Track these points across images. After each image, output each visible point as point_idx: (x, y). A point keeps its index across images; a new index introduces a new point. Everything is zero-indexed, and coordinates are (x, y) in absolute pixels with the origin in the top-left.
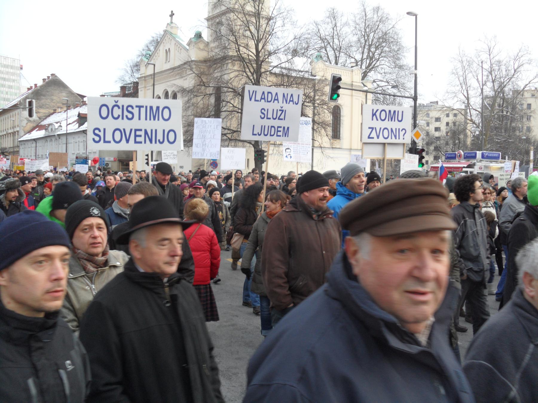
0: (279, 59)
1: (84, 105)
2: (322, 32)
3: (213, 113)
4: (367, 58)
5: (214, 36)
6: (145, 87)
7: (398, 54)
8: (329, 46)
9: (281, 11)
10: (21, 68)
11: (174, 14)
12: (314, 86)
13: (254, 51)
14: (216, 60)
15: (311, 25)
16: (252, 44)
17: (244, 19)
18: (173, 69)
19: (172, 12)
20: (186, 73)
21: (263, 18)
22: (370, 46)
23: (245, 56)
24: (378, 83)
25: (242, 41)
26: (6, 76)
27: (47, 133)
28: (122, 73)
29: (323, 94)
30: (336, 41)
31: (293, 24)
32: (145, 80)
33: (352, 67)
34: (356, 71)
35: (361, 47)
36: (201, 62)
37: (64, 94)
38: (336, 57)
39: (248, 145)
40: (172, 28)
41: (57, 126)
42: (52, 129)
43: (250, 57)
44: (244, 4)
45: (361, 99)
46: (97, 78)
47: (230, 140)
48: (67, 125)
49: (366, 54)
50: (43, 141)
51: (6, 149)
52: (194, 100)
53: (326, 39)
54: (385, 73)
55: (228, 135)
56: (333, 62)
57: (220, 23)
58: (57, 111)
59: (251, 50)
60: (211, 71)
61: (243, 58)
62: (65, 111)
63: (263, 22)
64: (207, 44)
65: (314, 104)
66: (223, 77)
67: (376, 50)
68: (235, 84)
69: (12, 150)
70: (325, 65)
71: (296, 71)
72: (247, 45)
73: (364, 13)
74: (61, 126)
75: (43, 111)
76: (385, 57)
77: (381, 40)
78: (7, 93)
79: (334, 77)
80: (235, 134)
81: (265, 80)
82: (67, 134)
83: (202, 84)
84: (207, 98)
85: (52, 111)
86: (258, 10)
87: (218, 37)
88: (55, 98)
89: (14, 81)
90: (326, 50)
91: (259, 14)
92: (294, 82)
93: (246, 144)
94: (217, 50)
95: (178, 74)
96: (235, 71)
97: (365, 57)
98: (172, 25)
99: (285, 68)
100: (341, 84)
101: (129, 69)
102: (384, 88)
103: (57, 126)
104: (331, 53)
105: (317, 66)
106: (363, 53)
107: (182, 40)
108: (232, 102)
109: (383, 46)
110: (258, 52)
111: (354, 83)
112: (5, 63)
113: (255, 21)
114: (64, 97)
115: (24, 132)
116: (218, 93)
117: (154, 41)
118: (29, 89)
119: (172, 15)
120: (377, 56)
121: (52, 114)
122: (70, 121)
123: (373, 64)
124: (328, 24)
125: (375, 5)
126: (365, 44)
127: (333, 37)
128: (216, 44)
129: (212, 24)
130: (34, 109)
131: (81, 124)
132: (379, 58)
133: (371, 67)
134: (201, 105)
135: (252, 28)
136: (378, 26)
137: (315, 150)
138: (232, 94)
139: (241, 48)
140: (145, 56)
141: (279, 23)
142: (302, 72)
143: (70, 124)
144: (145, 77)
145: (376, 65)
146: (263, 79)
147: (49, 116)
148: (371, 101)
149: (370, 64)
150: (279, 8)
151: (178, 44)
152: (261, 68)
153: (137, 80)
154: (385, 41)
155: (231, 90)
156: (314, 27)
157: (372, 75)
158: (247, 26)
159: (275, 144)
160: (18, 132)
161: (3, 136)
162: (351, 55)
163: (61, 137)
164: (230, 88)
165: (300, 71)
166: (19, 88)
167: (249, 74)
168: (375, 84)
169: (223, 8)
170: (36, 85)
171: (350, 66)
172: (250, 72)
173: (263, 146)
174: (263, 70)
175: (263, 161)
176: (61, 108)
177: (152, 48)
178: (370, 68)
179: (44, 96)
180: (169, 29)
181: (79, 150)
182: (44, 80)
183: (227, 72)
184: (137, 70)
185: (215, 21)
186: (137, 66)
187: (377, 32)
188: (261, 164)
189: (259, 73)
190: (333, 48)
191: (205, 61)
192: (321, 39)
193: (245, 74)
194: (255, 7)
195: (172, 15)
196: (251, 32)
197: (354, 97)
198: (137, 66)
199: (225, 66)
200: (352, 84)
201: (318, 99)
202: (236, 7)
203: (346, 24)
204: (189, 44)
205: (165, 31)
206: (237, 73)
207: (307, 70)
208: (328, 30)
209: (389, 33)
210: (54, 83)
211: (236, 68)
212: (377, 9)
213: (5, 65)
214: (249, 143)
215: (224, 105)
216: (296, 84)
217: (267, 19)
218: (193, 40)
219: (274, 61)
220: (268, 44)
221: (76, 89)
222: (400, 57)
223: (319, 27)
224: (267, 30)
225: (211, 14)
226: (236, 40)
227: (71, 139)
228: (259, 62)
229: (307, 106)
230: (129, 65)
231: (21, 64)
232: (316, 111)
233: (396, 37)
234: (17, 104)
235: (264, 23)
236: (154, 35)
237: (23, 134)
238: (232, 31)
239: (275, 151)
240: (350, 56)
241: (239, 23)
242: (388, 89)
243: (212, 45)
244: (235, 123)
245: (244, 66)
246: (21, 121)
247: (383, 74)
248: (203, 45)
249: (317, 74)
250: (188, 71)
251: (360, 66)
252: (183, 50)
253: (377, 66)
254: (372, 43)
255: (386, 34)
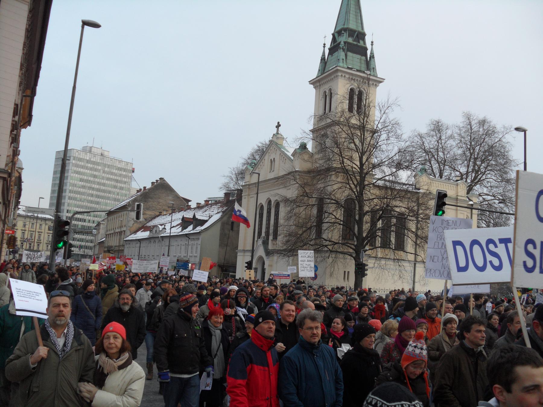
0: (383, 172)
1: (188, 209)
2: (426, 144)
3: (315, 224)
4: (473, 172)
5: (319, 148)
6: (249, 195)
7: (505, 167)
8: (433, 159)
9: (386, 125)
10: (133, 171)
11: (280, 126)
12: (418, 199)
13: (358, 163)
14: (320, 171)
15: (416, 138)
16: (356, 156)
17: (349, 132)
18: (277, 178)
19: (278, 123)
20: (290, 183)
21: (368, 130)
22: (476, 159)
23: (349, 168)
24: (484, 197)
25: (346, 153)
26: (119, 179)
27: (151, 234)
28: (226, 180)
29: (427, 208)
30: (441, 154)
31: (398, 137)
32: (249, 188)
33: (457, 181)
34: (461, 185)
35: (466, 160)
36: (304, 172)
37: (170, 198)
38: (441, 170)
39: (349, 257)
40: (278, 138)
41: (161, 228)
42: (156, 231)
43: (354, 169)
44: (349, 118)
45: (466, 213)
46: (202, 182)
47: (331, 251)
48: (171, 228)
49: (472, 168)
50: (147, 242)
51: (112, 247)
52: (296, 210)
53: (430, 152)
54: (491, 187)
55: (329, 247)
56: (438, 175)
57: (325, 136)
58: (162, 214)
59: (355, 162)
60: (315, 182)
61: (347, 170)
62: (170, 214)
63: (368, 135)
64: (312, 155)
65: (417, 218)
66: (326, 188)
67: (482, 164)
68: (338, 196)
69: (117, 249)
70: (429, 178)
71: (400, 184)
72: (351, 157)
73: (469, 127)
74: (165, 228)
75: (150, 213)
76: (491, 170)
77: (487, 154)
78: (118, 194)
79: (439, 193)
80: (336, 246)
81: (368, 193)
82: (170, 237)
83: (306, 194)
84: (310, 209)
85: (158, 214)
86: (363, 123)
87: (321, 148)
88: (161, 201)
89: (125, 183)
90: (430, 163)
91: (364, 127)
92: (397, 196)
93: (347, 256)
94: (321, 162)
95: (282, 184)
96: (339, 182)
97: (470, 170)
98: (279, 136)
99: (389, 181)
100: (447, 201)
101: (234, 176)
102: (490, 202)
103: (161, 228)
104: (435, 166)
105: (421, 180)
106: (468, 166)
107: (288, 152)
108: (334, 213)
109: (489, 160)
110: (362, 164)
111: (459, 198)
112: (119, 166)
113: (359, 134)
114: (170, 200)
115: (130, 232)
116: (321, 204)
117: (259, 150)
118: (138, 191)
119: (278, 126)
120: (483, 170)
121: (158, 216)
122: (174, 224)
123: (479, 177)
124: (433, 137)
125: (481, 117)
126: (471, 157)
127: (437, 149)
128: (321, 155)
129: (317, 137)
130: (142, 212)
131: (184, 228)
132: (485, 172)
133: (477, 180)
134: (303, 215)
135: (357, 141)
136: (484, 139)
137: (417, 265)
138: (334, 206)
139: (345, 160)
140: (250, 165)
141: (384, 136)
142: (406, 185)
143: (174, 227)
144: (249, 185)
145: (482, 179)
146: (366, 192)
147: (155, 218)
148: (476, 216)
149: (475, 178)
150: (384, 122)
151: (284, 155)
152: (364, 180)
153: (241, 187)
154: (491, 154)
155: (334, 202)
156: (419, 140)
157: (478, 188)
158: (351, 139)
159: (376, 258)
160: (124, 231)
161: (111, 234)
162: (456, 168)
163: (165, 240)
164: (332, 199)
165: (404, 184)
166: (129, 190)
167: (352, 186)
168: (481, 199)
169: (329, 121)
170: (145, 188)
171: (455, 179)
172: (354, 184)
173: (364, 259)
174: (366, 183)
175: (364, 275)
176: (167, 211)
177: (257, 157)
178: (475, 182)
179: (151, 198)
180: (275, 140)
181: (180, 253)
182: (153, 183)
183: (330, 183)
184: (242, 178)
185: (319, 133)
186: (241, 174)
187: (482, 145)
188: (362, 277)
189: (362, 186)
190: (438, 161)
191: (309, 172)
192: (426, 151)
193: (348, 186)
194: (360, 120)
195: (278, 126)
196: (355, 145)
197: (459, 212)
198: (242, 173)
199: (329, 177)
200: (457, 198)
201: (421, 214)
202: (342, 120)
203: (451, 137)
204: (293, 155)
205: (271, 141)
206: (340, 185)
207: (411, 183)
208: (433, 143)
209: (496, 146)
210: (161, 186)
211: (339, 180)
212: (483, 123)
213: (119, 168)
214: (350, 255)
215: (326, 216)
216: (400, 197)
217: (371, 132)
218: (298, 151)
219: (378, 174)
220: (372, 157)
221: (182, 193)
222: (508, 170)
223: (424, 140)
224: (371, 142)
225: (316, 127)
226: (341, 153)
227: (173, 242)
228: (363, 173)
229: (410, 220)
230: (234, 173)
231: (133, 167)
232: (419, 226)
233: (502, 150)
234: (126, 205)
235: (368, 136)
236: (260, 145)
237: (129, 233)
238: (336, 143)
239: (376, 265)
240: (455, 169)
241: (344, 136)
242: (495, 203)
243: (316, 156)
244: (336, 234)
245: (347, 178)
246: (128, 221)
247: (489, 188)
248: (308, 156)
249: (421, 188)
250: (292, 181)
251: (465, 180)
252: (287, 160)
253: (484, 180)
254: (477, 156)
255: (492, 147)
